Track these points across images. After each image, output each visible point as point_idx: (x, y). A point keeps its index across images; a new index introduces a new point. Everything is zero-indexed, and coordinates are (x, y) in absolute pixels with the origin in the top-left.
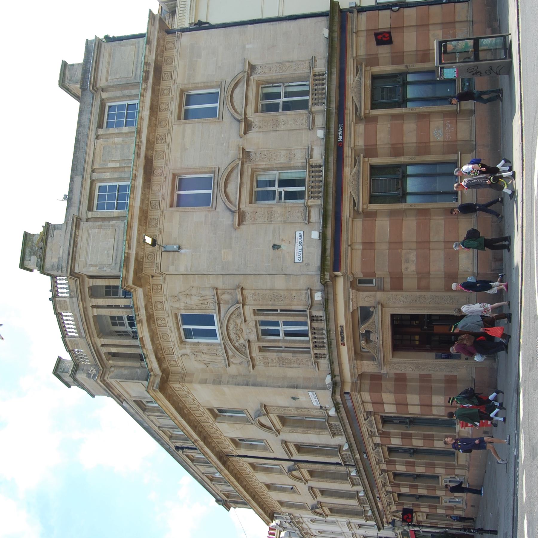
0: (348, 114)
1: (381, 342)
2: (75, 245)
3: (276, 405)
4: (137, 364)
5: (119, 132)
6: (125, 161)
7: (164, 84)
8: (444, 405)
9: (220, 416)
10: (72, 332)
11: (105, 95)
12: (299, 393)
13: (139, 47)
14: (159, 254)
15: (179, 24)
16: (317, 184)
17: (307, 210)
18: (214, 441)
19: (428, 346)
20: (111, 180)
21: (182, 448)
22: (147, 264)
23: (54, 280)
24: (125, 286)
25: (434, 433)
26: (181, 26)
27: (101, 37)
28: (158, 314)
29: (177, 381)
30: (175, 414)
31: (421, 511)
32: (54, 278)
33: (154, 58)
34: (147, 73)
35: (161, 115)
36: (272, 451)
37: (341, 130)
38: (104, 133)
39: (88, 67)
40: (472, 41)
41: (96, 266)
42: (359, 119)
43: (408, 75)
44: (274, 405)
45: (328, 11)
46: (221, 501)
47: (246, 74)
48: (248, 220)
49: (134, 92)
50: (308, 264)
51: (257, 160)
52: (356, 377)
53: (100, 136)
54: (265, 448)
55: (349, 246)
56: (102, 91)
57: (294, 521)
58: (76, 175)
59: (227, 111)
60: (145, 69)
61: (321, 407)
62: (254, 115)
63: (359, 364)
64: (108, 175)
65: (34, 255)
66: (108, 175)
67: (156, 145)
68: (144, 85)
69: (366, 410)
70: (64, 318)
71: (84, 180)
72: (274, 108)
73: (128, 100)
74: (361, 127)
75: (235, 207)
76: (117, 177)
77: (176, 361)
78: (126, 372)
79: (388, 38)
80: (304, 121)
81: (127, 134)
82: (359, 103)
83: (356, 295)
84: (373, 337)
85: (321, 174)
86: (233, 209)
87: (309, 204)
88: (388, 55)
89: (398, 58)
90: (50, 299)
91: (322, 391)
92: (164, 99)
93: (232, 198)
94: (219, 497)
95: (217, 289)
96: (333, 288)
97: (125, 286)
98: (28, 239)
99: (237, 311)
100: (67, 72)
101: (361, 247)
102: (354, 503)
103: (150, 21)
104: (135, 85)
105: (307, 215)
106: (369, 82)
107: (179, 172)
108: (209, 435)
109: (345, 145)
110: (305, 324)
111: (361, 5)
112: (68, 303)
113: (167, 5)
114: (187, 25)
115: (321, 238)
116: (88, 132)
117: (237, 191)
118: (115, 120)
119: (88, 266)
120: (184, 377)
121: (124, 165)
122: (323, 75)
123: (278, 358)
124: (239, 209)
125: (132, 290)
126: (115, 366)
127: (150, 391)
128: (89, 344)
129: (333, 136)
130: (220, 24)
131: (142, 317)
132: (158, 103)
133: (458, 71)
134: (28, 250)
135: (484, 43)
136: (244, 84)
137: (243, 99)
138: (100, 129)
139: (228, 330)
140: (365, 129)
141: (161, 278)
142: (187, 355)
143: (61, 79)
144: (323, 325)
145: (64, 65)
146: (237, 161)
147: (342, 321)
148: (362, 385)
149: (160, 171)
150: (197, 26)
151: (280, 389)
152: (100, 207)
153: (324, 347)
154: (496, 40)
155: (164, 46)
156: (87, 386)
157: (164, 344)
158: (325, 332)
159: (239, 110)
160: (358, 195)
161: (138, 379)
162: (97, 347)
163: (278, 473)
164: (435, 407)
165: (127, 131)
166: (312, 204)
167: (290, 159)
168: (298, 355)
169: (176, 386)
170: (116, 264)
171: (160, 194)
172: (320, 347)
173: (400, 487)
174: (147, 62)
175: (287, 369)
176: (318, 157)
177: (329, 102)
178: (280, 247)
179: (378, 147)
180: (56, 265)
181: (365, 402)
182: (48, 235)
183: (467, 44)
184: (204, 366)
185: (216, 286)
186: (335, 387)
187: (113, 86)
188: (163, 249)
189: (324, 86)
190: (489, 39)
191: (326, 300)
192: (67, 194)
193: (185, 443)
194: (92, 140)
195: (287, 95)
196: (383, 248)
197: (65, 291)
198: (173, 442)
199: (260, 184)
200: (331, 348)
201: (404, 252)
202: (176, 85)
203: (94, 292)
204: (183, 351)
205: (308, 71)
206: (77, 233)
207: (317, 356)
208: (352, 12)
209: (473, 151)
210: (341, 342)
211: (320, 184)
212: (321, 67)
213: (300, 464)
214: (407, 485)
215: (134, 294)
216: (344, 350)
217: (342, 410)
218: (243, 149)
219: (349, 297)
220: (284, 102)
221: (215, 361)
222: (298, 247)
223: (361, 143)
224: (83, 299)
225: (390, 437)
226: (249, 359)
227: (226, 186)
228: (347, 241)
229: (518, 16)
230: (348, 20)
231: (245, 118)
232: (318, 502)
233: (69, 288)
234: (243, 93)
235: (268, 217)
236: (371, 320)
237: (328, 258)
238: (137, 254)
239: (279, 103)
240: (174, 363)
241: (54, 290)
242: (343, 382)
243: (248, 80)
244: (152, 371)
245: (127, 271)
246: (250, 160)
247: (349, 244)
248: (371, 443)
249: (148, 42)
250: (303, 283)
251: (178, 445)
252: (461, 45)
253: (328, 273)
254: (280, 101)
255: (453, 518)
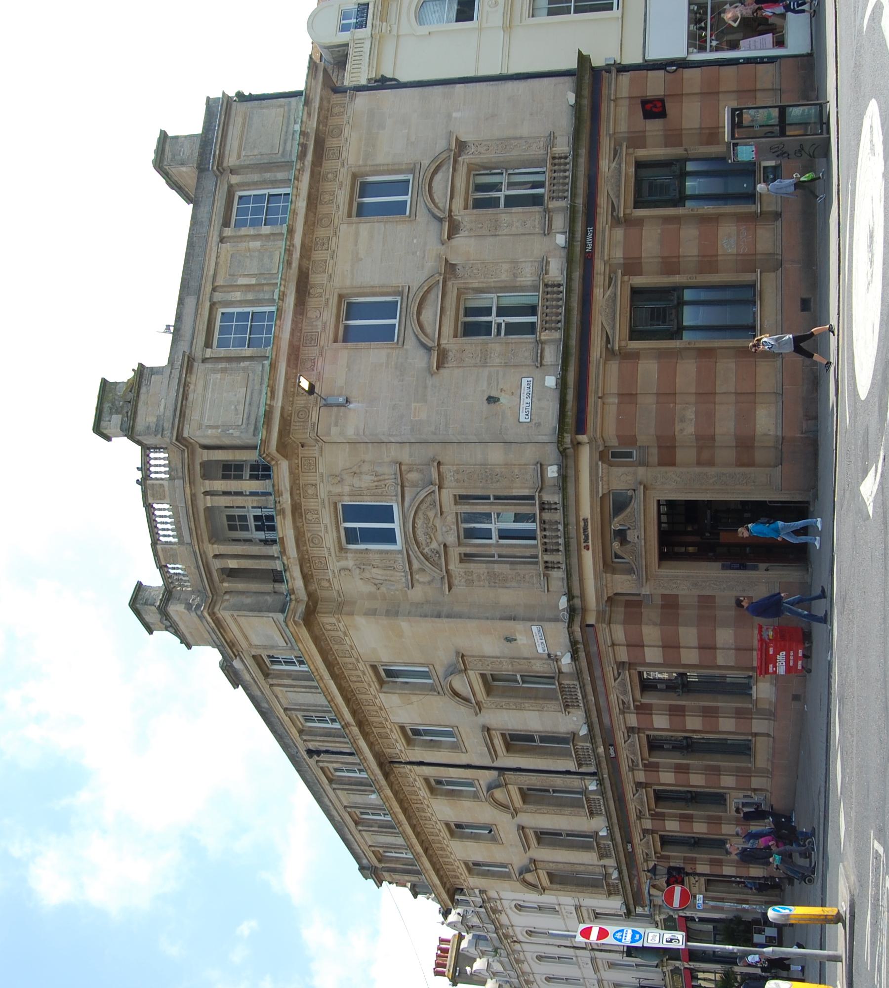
0: (600, 214)
1: (643, 542)
2: (185, 397)
3: (481, 654)
4: (268, 587)
5: (256, 233)
6: (265, 276)
7: (328, 165)
8: (733, 647)
9: (388, 682)
10: (168, 536)
11: (234, 179)
12: (518, 627)
13: (290, 110)
14: (316, 409)
15: (352, 79)
16: (554, 310)
17: (540, 348)
18: (373, 732)
19: (711, 554)
20: (241, 303)
21: (318, 753)
22: (297, 424)
23: (145, 452)
24: (264, 452)
25: (719, 704)
26: (354, 83)
27: (232, 93)
28: (309, 504)
29: (331, 613)
30: (322, 671)
31: (698, 871)
32: (146, 449)
33: (315, 125)
34: (304, 147)
35: (323, 210)
36: (464, 750)
37: (590, 235)
38: (233, 234)
39: (210, 137)
40: (777, 110)
41: (217, 427)
42: (617, 221)
43: (688, 163)
44: (477, 654)
45: (575, 69)
46: (368, 869)
47: (453, 153)
48: (451, 362)
49: (280, 176)
50: (538, 425)
51: (466, 276)
52: (604, 602)
53: (225, 239)
54: (455, 747)
55: (599, 398)
56: (231, 173)
57: (488, 905)
58: (189, 294)
59: (423, 206)
60: (302, 140)
61: (549, 655)
62: (463, 212)
63: (609, 579)
64: (237, 296)
65: (117, 413)
66: (237, 296)
67: (313, 252)
68: (299, 163)
69: (617, 660)
70: (157, 513)
71: (200, 301)
72: (492, 203)
73: (270, 188)
74: (619, 234)
75: (434, 341)
76: (251, 298)
77: (329, 581)
78: (248, 600)
79: (661, 109)
80: (537, 223)
81: (268, 236)
82: (617, 200)
83: (608, 473)
84: (631, 536)
85: (560, 296)
86: (430, 344)
87: (543, 338)
88: (661, 133)
89: (673, 137)
90: (138, 480)
91: (552, 624)
92: (328, 186)
93: (429, 330)
94: (365, 861)
95: (400, 464)
96: (575, 462)
97: (264, 452)
98: (107, 389)
99: (429, 498)
100: (167, 148)
101: (616, 401)
102: (588, 858)
103: (311, 72)
104: (288, 165)
105: (539, 355)
106: (632, 170)
107: (348, 291)
108: (367, 720)
109: (596, 256)
110: (531, 518)
111: (623, 63)
112: (166, 489)
113: (332, 53)
114: (364, 82)
115: (559, 387)
116: (208, 232)
117: (436, 320)
118: (249, 217)
119: (204, 427)
120: (342, 606)
121: (264, 282)
122: (566, 158)
123: (488, 573)
124: (439, 345)
125: (273, 463)
126: (231, 592)
127: (290, 624)
128: (195, 553)
129: (579, 243)
130: (414, 82)
131: (284, 506)
132: (318, 192)
133: (756, 150)
134: (107, 406)
135: (793, 114)
136: (449, 168)
137: (447, 190)
138: (227, 229)
139: (414, 527)
140: (625, 236)
141: (316, 448)
142: (348, 569)
143: (159, 158)
144: (558, 516)
145: (163, 136)
146: (437, 277)
147: (586, 511)
148: (612, 615)
149: (319, 291)
150: (379, 83)
151: (489, 622)
152: (222, 344)
153: (558, 550)
154: (809, 110)
155: (328, 109)
156: (182, 627)
157: (314, 552)
158: (561, 527)
159: (440, 205)
160: (614, 328)
161: (269, 611)
162: (206, 558)
163: (470, 798)
164: (721, 651)
165: (268, 232)
166: (546, 338)
167: (515, 276)
168: (518, 567)
169: (326, 620)
170: (248, 424)
171: (319, 323)
172: (553, 551)
173: (664, 820)
174: (304, 132)
175: (500, 590)
176: (556, 271)
177: (574, 195)
178: (498, 400)
179: (642, 260)
180: (153, 426)
181: (616, 645)
182: (142, 382)
183: (769, 114)
184: (373, 589)
185: (400, 460)
186: (573, 616)
187: (247, 167)
188: (323, 402)
189: (567, 174)
190: (800, 107)
191: (563, 477)
192: (173, 323)
193: (323, 741)
194: (214, 244)
195: (511, 185)
196: (648, 402)
197: (163, 469)
198: (305, 741)
199: (469, 312)
200: (569, 551)
201: (678, 407)
202: (346, 167)
203: (208, 470)
204: (343, 563)
205: (542, 152)
206: (188, 379)
207: (548, 566)
208: (609, 71)
209: (778, 270)
210: (583, 545)
211: (559, 311)
212: (563, 147)
213: (509, 776)
214: (675, 816)
215: (275, 468)
216: (588, 557)
217: (582, 654)
218: (446, 260)
219: (597, 474)
220: (506, 196)
221: (392, 579)
222: (525, 400)
223: (618, 254)
224: (191, 481)
225: (651, 714)
226: (445, 574)
227: (419, 313)
228: (596, 392)
229: (837, 76)
230: (604, 82)
231: (450, 216)
232: (531, 859)
233: (169, 465)
234: (447, 181)
235: (481, 358)
236: (629, 510)
237: (569, 413)
238: (283, 408)
239: (500, 197)
240: (327, 584)
241: (145, 468)
242: (584, 610)
243: (455, 161)
244: (294, 593)
245: (269, 431)
246: (456, 277)
247: (600, 395)
248: (623, 726)
249: (307, 103)
250: (529, 454)
251: (312, 746)
252: (761, 116)
253: (569, 435)
254: (501, 195)
255: (749, 886)
